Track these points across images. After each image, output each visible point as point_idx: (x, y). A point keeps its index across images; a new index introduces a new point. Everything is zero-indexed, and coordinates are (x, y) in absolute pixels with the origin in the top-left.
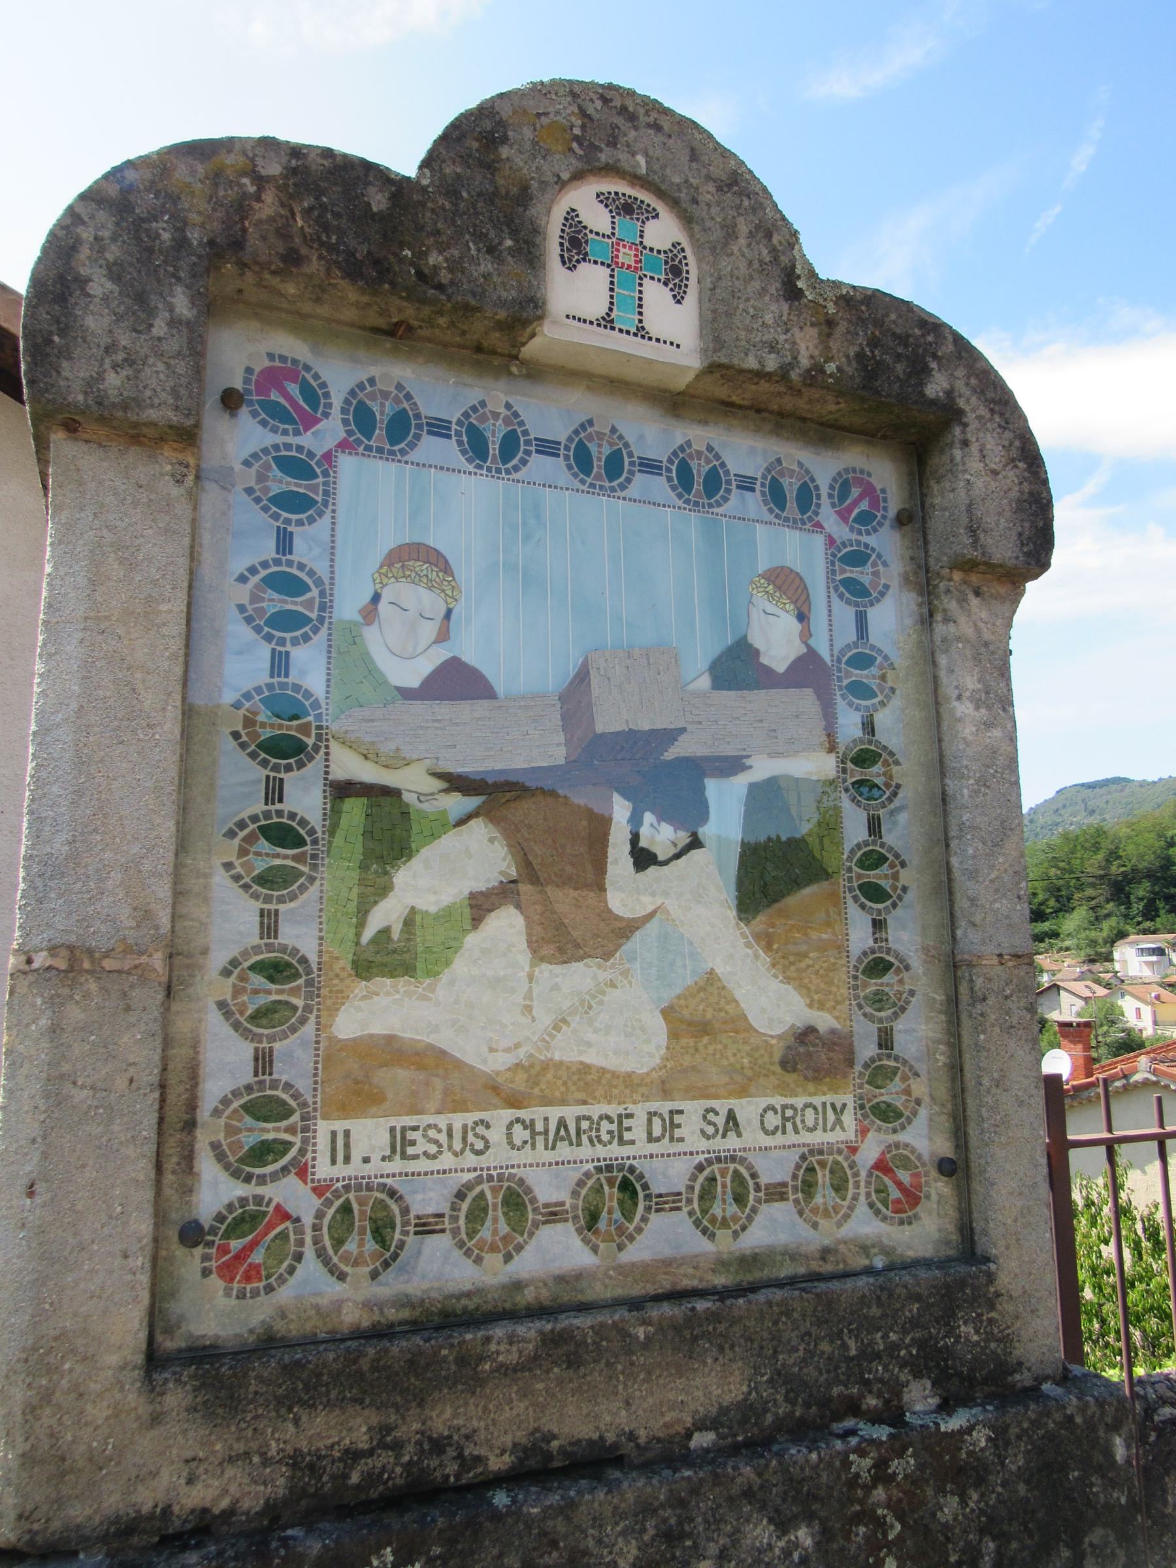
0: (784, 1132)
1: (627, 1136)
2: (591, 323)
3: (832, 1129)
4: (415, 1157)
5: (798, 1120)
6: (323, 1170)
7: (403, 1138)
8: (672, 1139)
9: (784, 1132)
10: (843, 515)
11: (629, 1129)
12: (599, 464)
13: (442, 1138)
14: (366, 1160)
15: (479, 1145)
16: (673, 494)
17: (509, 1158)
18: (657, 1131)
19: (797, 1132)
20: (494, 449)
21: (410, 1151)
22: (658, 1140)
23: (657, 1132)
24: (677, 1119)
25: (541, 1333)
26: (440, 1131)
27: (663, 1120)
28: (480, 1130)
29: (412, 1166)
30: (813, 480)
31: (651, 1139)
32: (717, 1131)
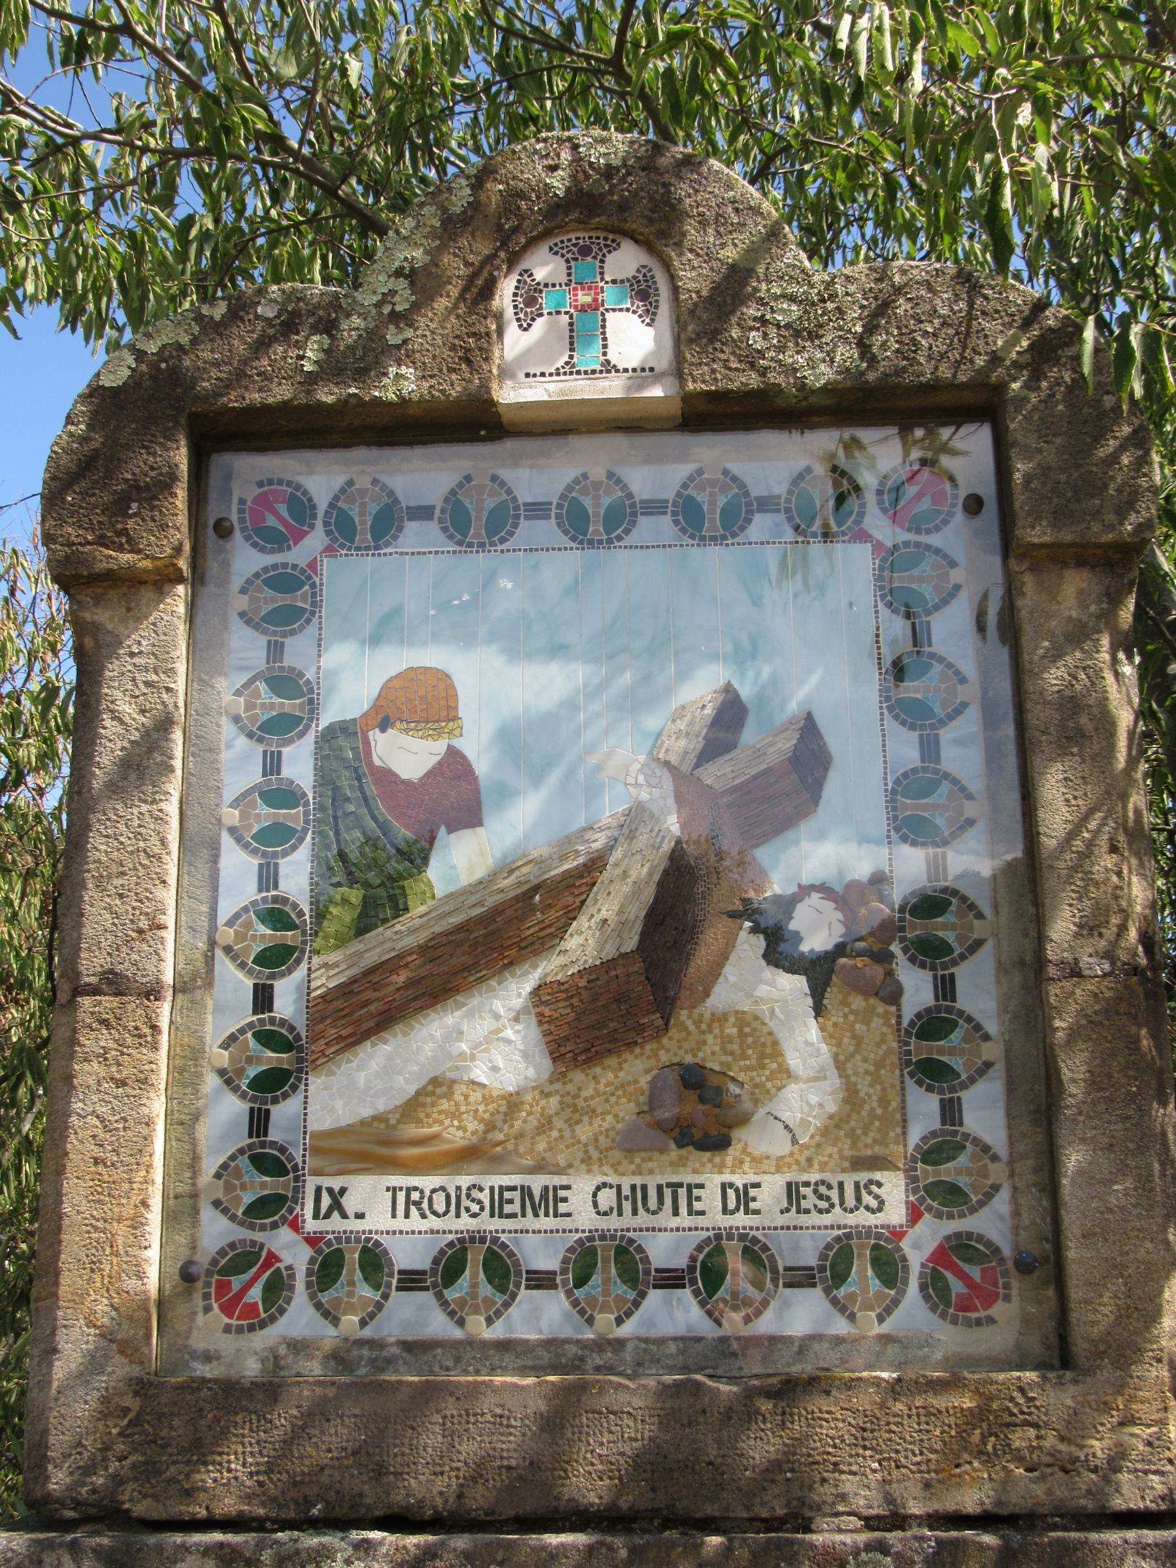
0: (620, 1214)
1: (697, 1206)
2: (605, 354)
3: (327, 1215)
4: (807, 1211)
5: (425, 1205)
6: (311, 1225)
7: (555, 1196)
8: (798, 1212)
9: (620, 1214)
10: (299, 536)
11: (565, 1200)
12: (595, 523)
13: (834, 1195)
14: (360, 1216)
15: (874, 1203)
16: (566, 538)
17: (773, 1220)
18: (732, 1205)
19: (423, 1216)
20: (480, 525)
21: (563, 1207)
22: (732, 1213)
23: (732, 1205)
24: (752, 1192)
25: (256, 1304)
26: (830, 1187)
27: (448, 1197)
28: (874, 1188)
29: (803, 1219)
30: (257, 575)
31: (725, 1210)
32: (482, 1209)
